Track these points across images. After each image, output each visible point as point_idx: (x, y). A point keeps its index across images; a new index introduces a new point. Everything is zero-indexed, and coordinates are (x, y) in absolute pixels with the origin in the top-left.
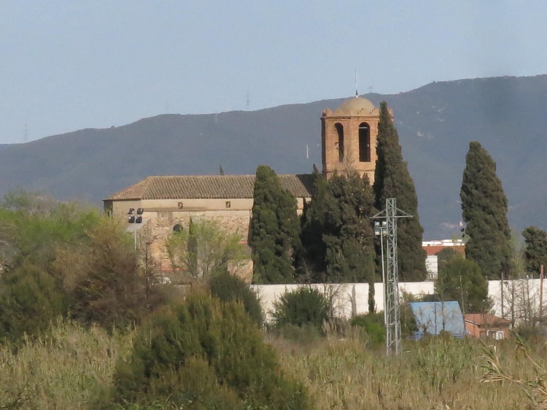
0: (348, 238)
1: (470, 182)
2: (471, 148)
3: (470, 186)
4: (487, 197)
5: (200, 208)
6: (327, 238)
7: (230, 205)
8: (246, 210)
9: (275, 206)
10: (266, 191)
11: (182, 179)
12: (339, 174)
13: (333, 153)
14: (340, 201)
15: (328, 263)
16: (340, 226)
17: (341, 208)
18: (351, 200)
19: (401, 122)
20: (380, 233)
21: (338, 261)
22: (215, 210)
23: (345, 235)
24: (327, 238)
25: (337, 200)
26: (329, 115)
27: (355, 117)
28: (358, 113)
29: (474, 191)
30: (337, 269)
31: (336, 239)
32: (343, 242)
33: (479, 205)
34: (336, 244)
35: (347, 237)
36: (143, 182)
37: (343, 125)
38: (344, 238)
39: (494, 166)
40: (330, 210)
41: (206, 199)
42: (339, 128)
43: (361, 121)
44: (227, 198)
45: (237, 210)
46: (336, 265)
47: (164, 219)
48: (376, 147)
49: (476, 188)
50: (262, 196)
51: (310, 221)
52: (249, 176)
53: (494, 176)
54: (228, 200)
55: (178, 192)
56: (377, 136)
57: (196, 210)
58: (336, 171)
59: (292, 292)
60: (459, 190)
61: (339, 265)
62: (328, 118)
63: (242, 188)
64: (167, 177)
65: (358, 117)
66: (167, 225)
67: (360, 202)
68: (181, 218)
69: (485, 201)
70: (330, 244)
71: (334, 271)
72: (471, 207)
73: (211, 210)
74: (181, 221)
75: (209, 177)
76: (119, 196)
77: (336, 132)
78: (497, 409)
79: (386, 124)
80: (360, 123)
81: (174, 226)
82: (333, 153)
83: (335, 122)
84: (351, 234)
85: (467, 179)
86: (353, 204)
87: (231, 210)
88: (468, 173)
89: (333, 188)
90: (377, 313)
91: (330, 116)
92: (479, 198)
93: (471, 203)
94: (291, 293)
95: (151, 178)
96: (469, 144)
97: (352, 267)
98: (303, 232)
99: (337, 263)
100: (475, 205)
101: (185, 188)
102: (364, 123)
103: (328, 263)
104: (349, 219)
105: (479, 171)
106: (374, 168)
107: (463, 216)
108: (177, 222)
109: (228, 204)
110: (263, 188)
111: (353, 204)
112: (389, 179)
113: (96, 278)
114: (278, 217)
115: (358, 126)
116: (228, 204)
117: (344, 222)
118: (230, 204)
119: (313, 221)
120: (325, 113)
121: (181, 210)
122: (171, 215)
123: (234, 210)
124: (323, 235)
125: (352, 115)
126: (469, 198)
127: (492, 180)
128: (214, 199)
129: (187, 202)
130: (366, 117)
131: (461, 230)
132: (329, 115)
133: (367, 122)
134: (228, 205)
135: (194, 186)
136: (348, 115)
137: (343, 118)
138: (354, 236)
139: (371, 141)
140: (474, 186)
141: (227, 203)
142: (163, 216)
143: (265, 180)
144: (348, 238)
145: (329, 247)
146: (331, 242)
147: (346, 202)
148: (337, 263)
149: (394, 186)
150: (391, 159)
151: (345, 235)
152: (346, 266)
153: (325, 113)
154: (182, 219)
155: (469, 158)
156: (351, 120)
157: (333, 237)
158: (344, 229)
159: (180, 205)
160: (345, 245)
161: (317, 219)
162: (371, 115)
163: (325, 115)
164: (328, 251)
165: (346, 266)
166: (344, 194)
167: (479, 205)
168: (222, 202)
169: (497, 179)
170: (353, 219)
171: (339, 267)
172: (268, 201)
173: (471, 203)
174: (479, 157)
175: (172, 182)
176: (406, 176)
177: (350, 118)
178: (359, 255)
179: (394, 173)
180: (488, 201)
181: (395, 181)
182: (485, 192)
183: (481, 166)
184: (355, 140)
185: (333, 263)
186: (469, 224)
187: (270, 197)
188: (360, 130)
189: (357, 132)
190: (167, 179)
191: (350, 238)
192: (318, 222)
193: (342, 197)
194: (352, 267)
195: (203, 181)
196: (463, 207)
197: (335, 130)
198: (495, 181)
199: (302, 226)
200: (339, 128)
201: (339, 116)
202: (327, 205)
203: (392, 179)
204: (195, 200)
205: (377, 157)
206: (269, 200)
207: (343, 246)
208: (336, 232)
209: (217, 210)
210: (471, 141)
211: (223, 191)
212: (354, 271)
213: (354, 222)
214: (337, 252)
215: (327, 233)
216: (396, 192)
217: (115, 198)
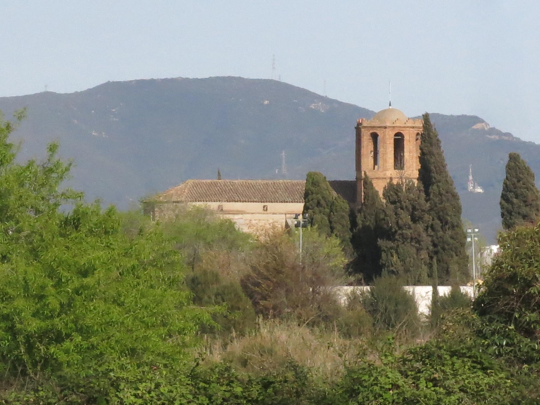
0: (403, 243)
1: (510, 191)
2: (510, 159)
3: (510, 195)
4: (526, 206)
5: (238, 211)
6: (381, 242)
7: (267, 209)
8: (282, 214)
9: (328, 210)
10: (320, 196)
11: (219, 183)
12: (395, 182)
13: (367, 161)
14: (396, 208)
15: (383, 265)
16: (396, 232)
17: (396, 214)
18: (406, 207)
19: (76, 121)
20: (472, 240)
21: (393, 264)
22: (252, 213)
23: (401, 240)
24: (381, 242)
25: (393, 206)
26: (365, 124)
27: (390, 127)
28: (405, 123)
29: (515, 201)
30: (393, 272)
31: (390, 244)
32: (398, 246)
33: (519, 213)
34: (391, 248)
35: (402, 242)
36: (182, 186)
37: (379, 133)
38: (399, 243)
39: (533, 176)
40: (386, 215)
41: (244, 203)
42: (375, 137)
44: (264, 202)
45: (274, 214)
46: (391, 268)
48: (419, 157)
49: (517, 198)
50: (316, 201)
51: (361, 226)
52: (282, 181)
53: (533, 186)
55: (218, 196)
56: (420, 146)
57: (235, 213)
58: (391, 179)
59: (443, 295)
60: (499, 199)
61: (395, 268)
62: (365, 127)
63: (278, 193)
64: (204, 181)
65: (394, 127)
67: (414, 208)
69: (525, 210)
70: (386, 249)
71: (390, 273)
72: (511, 215)
73: (248, 213)
75: (244, 181)
77: (371, 141)
78: (297, 404)
79: (429, 134)
83: (372, 131)
84: (407, 239)
85: (506, 188)
86: (408, 210)
87: (268, 214)
88: (508, 183)
89: (389, 194)
91: (366, 125)
92: (519, 207)
93: (511, 212)
94: (442, 297)
95: (190, 182)
96: (508, 156)
97: (407, 271)
98: (354, 236)
99: (392, 266)
100: (515, 213)
101: (224, 192)
102: (398, 132)
103: (383, 265)
104: (405, 225)
105: (519, 181)
106: (417, 176)
107: (503, 224)
109: (265, 208)
110: (317, 194)
111: (408, 210)
112: (435, 187)
113: (267, 279)
114: (330, 222)
115: (393, 135)
116: (265, 208)
117: (400, 228)
118: (267, 208)
119: (364, 227)
120: (360, 122)
123: (270, 213)
124: (379, 239)
125: (388, 124)
126: (510, 207)
127: (531, 190)
128: (252, 203)
129: (228, 206)
130: (400, 127)
132: (365, 124)
133: (401, 132)
134: (265, 209)
135: (232, 190)
137: (380, 127)
138: (409, 241)
139: (405, 150)
140: (514, 195)
141: (264, 207)
143: (319, 186)
144: (403, 243)
145: (384, 251)
146: (386, 247)
147: (402, 208)
148: (392, 266)
149: (440, 194)
150: (438, 169)
151: (401, 240)
152: (401, 269)
153: (360, 122)
155: (509, 168)
156: (387, 130)
157: (388, 242)
158: (400, 234)
160: (400, 250)
161: (367, 224)
162: (405, 125)
163: (361, 125)
164: (383, 255)
165: (401, 269)
166: (400, 201)
167: (519, 213)
169: (536, 189)
170: (409, 225)
171: (395, 270)
172: (321, 206)
173: (511, 212)
174: (519, 168)
175: (210, 186)
176: (451, 185)
177: (385, 128)
178: (414, 259)
179: (439, 182)
180: (528, 209)
181: (441, 189)
182: (525, 202)
183: (521, 176)
184: (390, 149)
185: (388, 266)
187: (322, 202)
188: (395, 139)
190: (205, 183)
191: (405, 243)
192: (369, 226)
193: (398, 204)
194: (407, 271)
195: (239, 185)
196: (503, 215)
197: (369, 139)
198: (535, 190)
199: (351, 230)
200: (375, 137)
202: (384, 211)
203: (438, 186)
204: (234, 203)
205: (420, 165)
206: (322, 205)
207: (399, 250)
208: (389, 235)
209: (276, 214)
211: (259, 195)
212: (409, 274)
213: (410, 228)
214: (392, 256)
215: (382, 238)
216: (441, 199)
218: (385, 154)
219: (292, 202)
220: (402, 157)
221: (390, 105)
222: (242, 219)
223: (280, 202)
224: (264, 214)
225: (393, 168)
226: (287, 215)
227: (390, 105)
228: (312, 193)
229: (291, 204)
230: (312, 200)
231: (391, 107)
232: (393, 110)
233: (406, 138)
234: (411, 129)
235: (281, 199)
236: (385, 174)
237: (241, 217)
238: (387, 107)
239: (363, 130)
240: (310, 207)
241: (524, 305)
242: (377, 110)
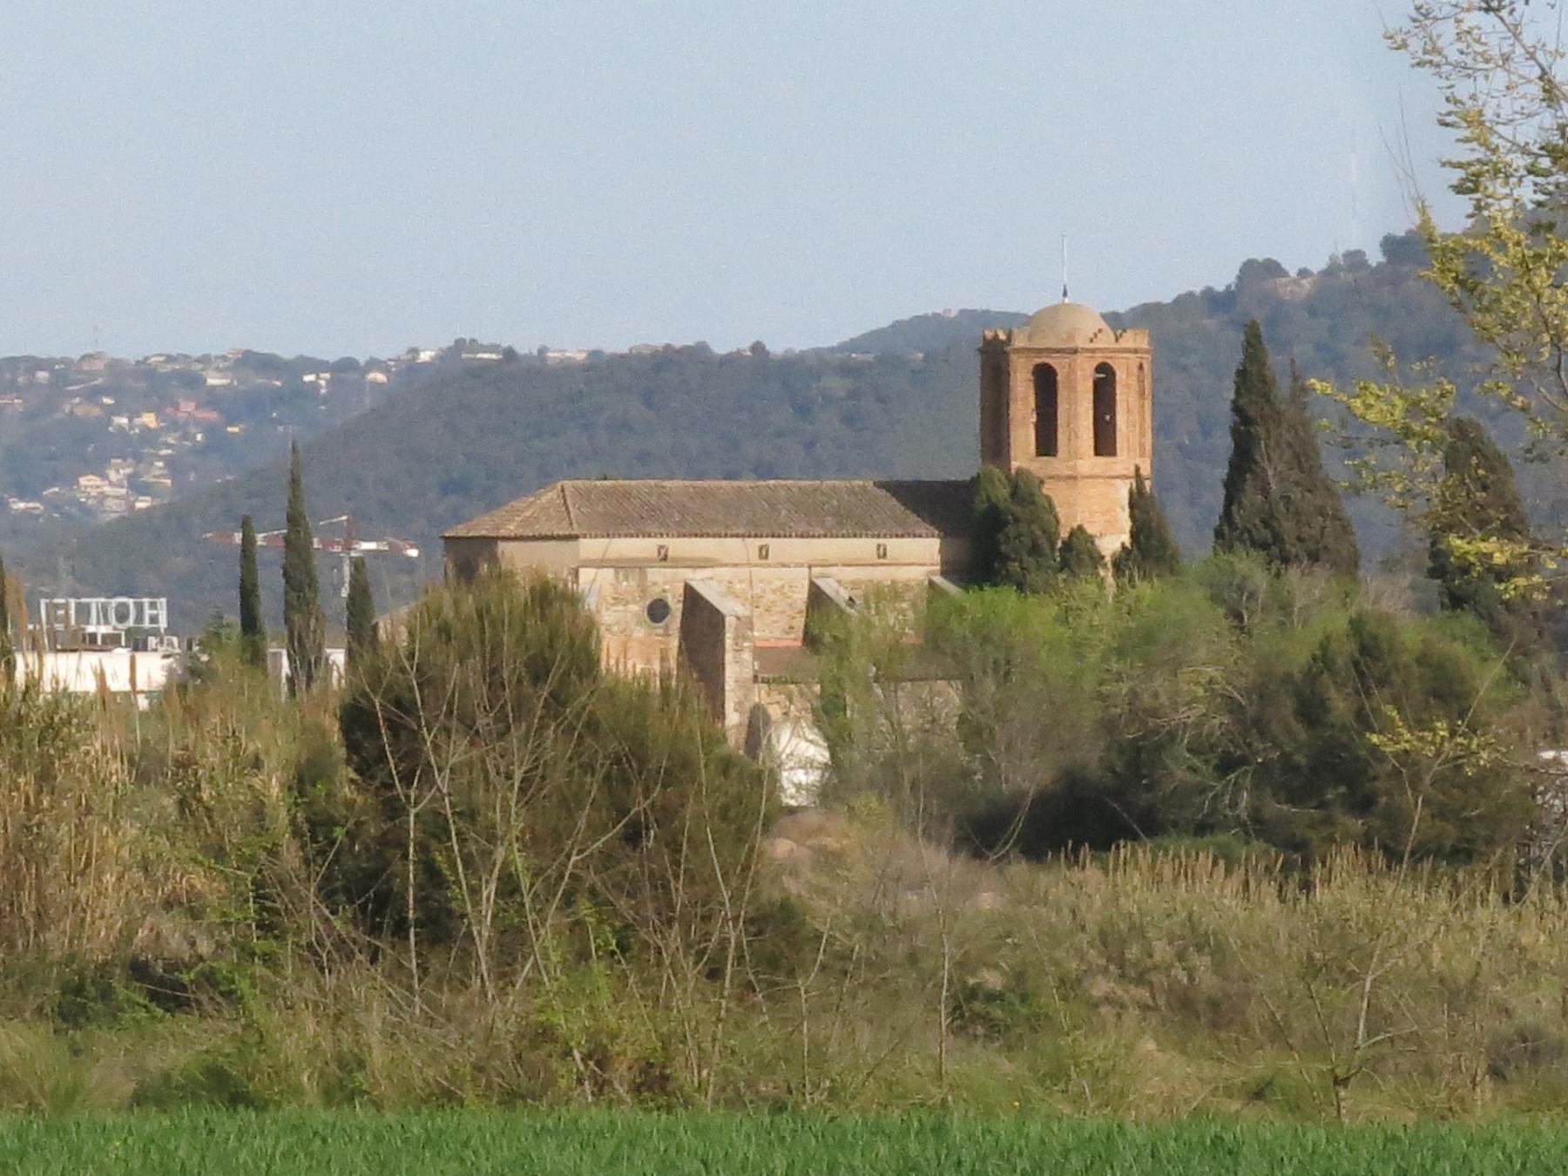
5: (708, 560)
8: (802, 565)
22: (736, 565)
37: (1055, 366)
43: (1099, 358)
45: (784, 565)
47: (629, 585)
50: (1027, 540)
54: (881, 541)
62: (1018, 351)
65: (1093, 351)
66: (636, 603)
68: (666, 583)
73: (727, 565)
74: (664, 591)
76: (512, 527)
80: (1095, 364)
81: (648, 602)
82: (1023, 436)
83: (1038, 361)
87: (769, 566)
90: (963, 854)
108: (655, 593)
109: (764, 553)
116: (764, 553)
121: (663, 563)
122: (643, 575)
125: (1081, 343)
129: (679, 546)
131: (248, 517)
133: (1109, 361)
136: (1071, 345)
137: (1058, 351)
141: (761, 548)
142: (627, 579)
154: (667, 587)
159: (663, 552)
168: (749, 547)
177: (1075, 351)
186: (162, 427)
189: (1090, 384)
200: (1046, 380)
201: (1049, 345)
210: (1211, 284)
217: (503, 532)
218: (1073, 417)
219: (825, 536)
220: (1112, 424)
221: (1065, 294)
222: (712, 578)
223: (797, 536)
224: (760, 566)
225: (1092, 452)
226: (814, 569)
227: (1065, 294)
228: (1017, 520)
229: (823, 540)
230: (1017, 537)
231: (1067, 301)
232: (1074, 307)
233: (1120, 376)
234: (1132, 356)
235: (801, 529)
236: (1074, 468)
237: (711, 575)
238: (1057, 299)
239: (1013, 357)
240: (1013, 555)
241: (143, 703)
242: (1030, 310)
